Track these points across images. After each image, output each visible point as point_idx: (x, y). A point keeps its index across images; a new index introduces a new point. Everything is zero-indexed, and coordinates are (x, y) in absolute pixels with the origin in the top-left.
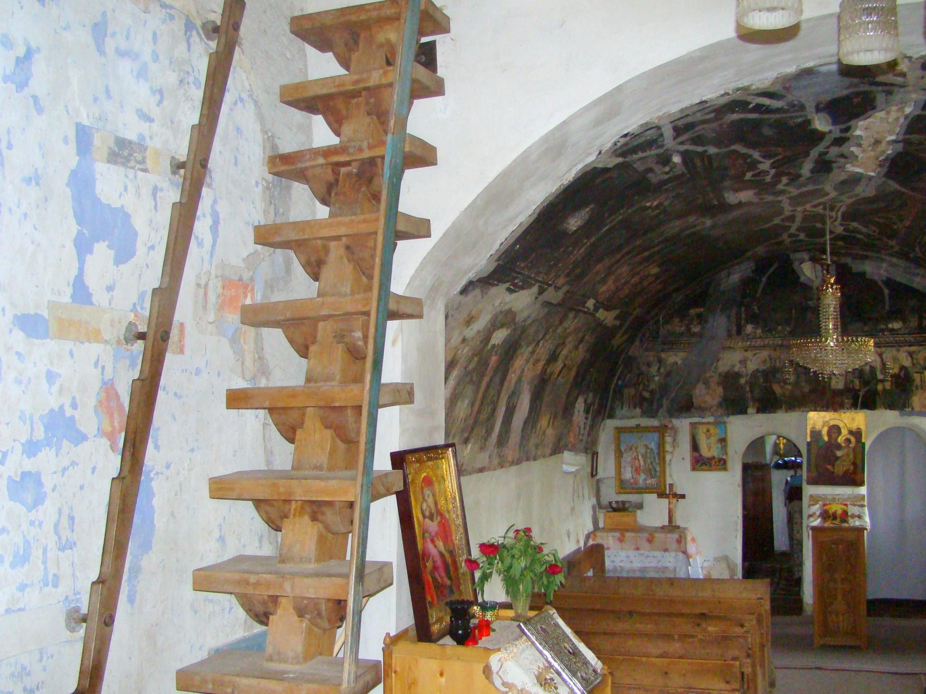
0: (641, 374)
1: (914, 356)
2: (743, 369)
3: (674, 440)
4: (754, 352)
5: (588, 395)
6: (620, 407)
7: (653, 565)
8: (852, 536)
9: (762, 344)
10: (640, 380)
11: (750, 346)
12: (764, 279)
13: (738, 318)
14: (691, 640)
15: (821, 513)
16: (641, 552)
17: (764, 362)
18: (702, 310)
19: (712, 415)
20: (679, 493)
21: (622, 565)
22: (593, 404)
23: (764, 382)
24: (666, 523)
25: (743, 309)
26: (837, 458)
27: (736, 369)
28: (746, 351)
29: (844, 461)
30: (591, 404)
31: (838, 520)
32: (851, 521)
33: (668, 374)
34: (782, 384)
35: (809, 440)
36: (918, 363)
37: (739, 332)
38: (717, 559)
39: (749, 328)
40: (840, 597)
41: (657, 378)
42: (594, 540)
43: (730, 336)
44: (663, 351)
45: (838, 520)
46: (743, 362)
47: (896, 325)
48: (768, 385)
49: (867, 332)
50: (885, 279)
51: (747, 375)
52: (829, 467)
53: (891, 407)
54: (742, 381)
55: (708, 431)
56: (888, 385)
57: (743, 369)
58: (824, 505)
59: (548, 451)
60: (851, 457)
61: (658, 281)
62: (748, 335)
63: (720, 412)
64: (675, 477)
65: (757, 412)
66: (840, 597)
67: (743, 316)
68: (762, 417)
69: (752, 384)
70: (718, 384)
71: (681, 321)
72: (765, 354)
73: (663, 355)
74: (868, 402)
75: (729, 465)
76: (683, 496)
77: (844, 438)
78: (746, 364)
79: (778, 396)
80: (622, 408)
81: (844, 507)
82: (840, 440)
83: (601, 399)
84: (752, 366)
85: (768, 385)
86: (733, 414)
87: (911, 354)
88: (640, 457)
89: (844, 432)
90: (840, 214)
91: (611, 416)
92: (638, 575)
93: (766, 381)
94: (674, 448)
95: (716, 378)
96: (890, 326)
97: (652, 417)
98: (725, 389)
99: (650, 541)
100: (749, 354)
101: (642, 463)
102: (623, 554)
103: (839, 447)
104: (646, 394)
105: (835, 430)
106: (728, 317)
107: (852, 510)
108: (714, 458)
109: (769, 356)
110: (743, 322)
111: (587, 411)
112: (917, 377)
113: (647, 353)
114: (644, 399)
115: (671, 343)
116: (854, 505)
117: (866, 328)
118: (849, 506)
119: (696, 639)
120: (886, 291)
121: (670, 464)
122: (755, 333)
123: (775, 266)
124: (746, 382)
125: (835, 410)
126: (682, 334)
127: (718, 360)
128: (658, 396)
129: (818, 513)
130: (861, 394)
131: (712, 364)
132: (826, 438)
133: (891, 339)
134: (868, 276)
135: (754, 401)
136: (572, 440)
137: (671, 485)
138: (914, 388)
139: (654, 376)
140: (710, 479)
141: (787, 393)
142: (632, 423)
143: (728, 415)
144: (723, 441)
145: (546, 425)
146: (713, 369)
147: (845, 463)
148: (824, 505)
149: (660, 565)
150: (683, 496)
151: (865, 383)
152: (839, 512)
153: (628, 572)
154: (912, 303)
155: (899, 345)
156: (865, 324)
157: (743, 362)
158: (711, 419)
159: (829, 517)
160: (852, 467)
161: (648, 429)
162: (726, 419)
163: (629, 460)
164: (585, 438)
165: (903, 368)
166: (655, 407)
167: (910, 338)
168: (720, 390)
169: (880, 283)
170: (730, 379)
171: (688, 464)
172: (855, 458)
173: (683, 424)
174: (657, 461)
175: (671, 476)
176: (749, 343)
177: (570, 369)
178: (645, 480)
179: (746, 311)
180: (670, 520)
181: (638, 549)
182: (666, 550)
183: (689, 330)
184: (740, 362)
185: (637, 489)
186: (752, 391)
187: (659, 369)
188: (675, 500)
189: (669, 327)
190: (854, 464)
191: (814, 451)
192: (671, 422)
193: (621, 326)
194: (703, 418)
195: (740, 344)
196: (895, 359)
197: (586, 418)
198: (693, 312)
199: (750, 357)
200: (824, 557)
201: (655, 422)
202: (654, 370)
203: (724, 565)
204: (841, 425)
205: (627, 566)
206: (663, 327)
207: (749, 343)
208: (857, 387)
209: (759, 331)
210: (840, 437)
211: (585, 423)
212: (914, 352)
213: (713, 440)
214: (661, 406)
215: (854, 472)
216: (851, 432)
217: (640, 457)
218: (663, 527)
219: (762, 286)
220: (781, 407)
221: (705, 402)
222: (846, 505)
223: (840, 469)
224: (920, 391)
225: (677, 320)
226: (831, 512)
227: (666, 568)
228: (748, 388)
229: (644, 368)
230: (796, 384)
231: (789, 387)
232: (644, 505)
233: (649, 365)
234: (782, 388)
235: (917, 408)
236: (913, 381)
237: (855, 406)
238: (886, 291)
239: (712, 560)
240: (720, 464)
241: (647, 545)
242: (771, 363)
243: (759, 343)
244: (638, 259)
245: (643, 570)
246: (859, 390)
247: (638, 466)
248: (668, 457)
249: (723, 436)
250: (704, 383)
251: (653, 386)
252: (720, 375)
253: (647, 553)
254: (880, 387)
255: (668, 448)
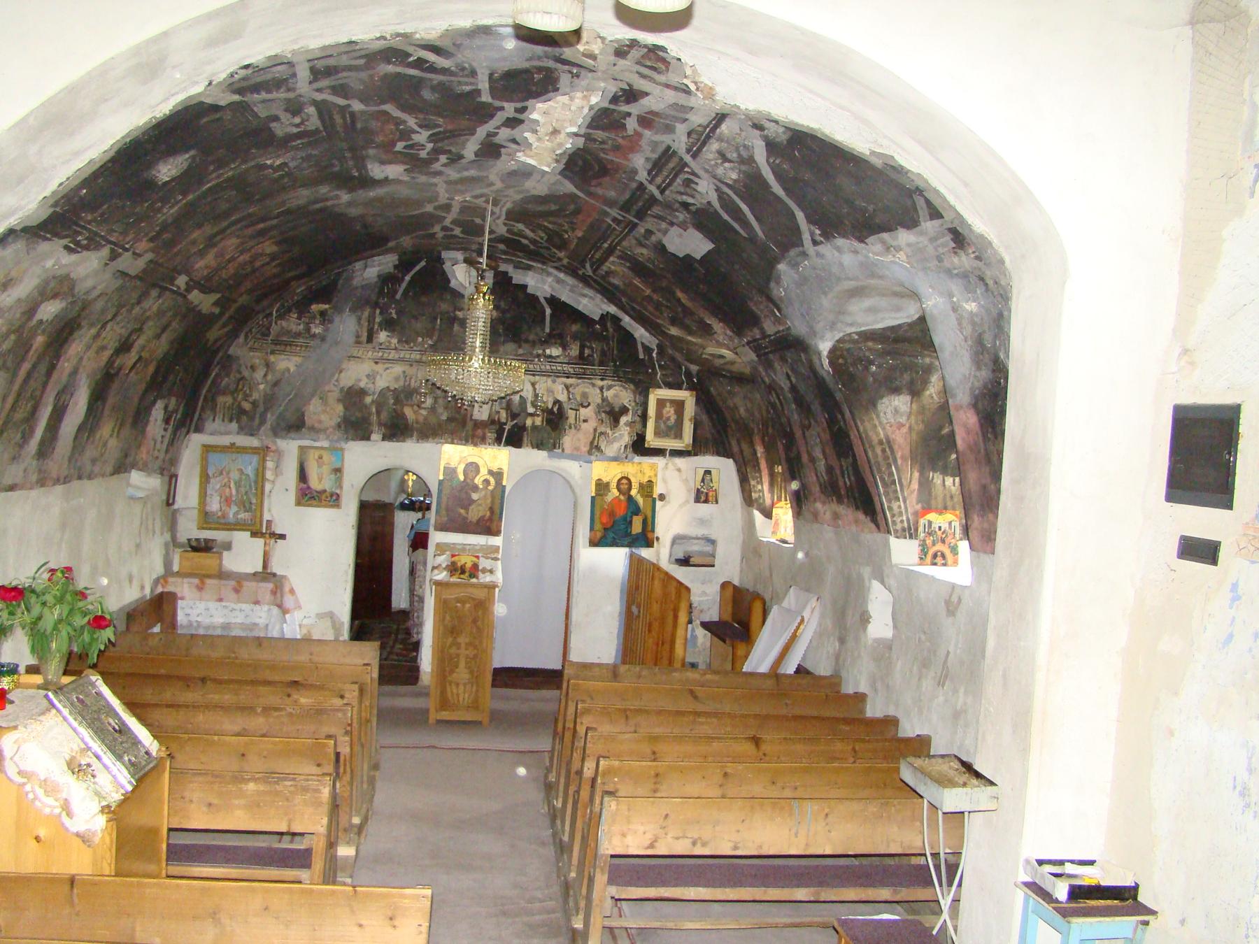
0: (243, 378)
1: (571, 389)
2: (371, 386)
3: (277, 467)
4: (386, 366)
5: (169, 400)
6: (212, 418)
7: (239, 620)
8: (480, 594)
9: (397, 356)
10: (240, 387)
11: (382, 358)
12: (408, 278)
13: (371, 320)
14: (276, 714)
15: (447, 566)
16: (224, 604)
17: (397, 379)
18: (327, 306)
19: (327, 438)
20: (278, 532)
21: (199, 619)
22: (176, 411)
23: (394, 404)
24: (260, 569)
25: (378, 311)
26: (474, 501)
27: (362, 385)
28: (376, 363)
29: (480, 505)
30: (173, 412)
31: (467, 574)
32: (481, 575)
33: (276, 384)
34: (415, 407)
35: (441, 477)
36: (575, 399)
37: (370, 339)
38: (320, 616)
39: (383, 336)
40: (462, 664)
41: (262, 387)
42: (163, 586)
43: (358, 342)
44: (273, 352)
45: (467, 574)
46: (371, 377)
47: (555, 351)
48: (398, 407)
49: (520, 355)
50: (548, 296)
51: (374, 393)
52: (462, 511)
53: (539, 446)
54: (368, 400)
55: (321, 457)
56: (538, 421)
57: (371, 386)
58: (453, 556)
59: (109, 469)
60: (489, 501)
61: (274, 264)
62: (381, 344)
63: (338, 434)
64: (274, 511)
65: (383, 439)
66: (462, 664)
67: (378, 320)
68: (387, 444)
69: (380, 405)
70: (339, 400)
71: (299, 318)
72: (398, 369)
73: (272, 358)
74: (514, 439)
75: (344, 500)
76: (282, 537)
77: (482, 479)
78: (374, 379)
79: (410, 421)
80: (214, 420)
81: (474, 559)
82: (478, 481)
83: (186, 405)
84: (381, 383)
85: (398, 407)
86: (353, 440)
87: (567, 387)
88: (232, 485)
89: (484, 471)
90: (504, 210)
91: (199, 429)
92: (219, 632)
93: (397, 401)
94: (277, 476)
95: (336, 394)
96: (548, 352)
97: (252, 435)
98: (346, 408)
99: (237, 591)
100: (380, 368)
101: (234, 492)
102: (201, 606)
103: (475, 488)
104: (247, 406)
105: (473, 468)
106: (359, 319)
107: (484, 563)
108: (325, 491)
109: (404, 372)
110: (376, 327)
111: (167, 421)
112: (571, 414)
113: (252, 354)
114: (242, 412)
115: (283, 343)
116: (487, 558)
117: (521, 351)
118: (482, 559)
119: (283, 713)
120: (548, 311)
121: (269, 496)
122: (390, 342)
123: (423, 263)
124: (373, 401)
125: (475, 445)
126: (298, 335)
127: (341, 372)
128: (261, 408)
129: (444, 566)
130: (507, 428)
131: (333, 375)
132: (462, 478)
133: (548, 367)
134: (529, 290)
135: (380, 424)
136: (144, 456)
137: (269, 522)
138: (567, 427)
139: (259, 384)
140: (319, 516)
141: (421, 419)
142: (225, 440)
143: (347, 439)
144: (338, 471)
145: (107, 436)
146: (333, 381)
147: (480, 508)
148: (453, 556)
149: (248, 621)
150: (282, 537)
151: (514, 416)
152: (469, 565)
153: (208, 628)
154: (575, 328)
155: (557, 374)
156: (520, 347)
157: (371, 377)
158: (326, 444)
159: (456, 570)
160: (488, 514)
161: (243, 450)
162: (343, 445)
163: (218, 486)
164: (162, 455)
165: (557, 402)
166: (257, 421)
167: (567, 368)
168: (340, 409)
169: (542, 301)
170: (353, 396)
171: (292, 496)
172: (493, 502)
173: (290, 447)
174: (254, 491)
175: (269, 510)
176: (380, 354)
177: (147, 362)
178: (236, 513)
179: (381, 313)
180: (265, 566)
181: (221, 600)
182: (257, 602)
183: (308, 330)
184: (368, 376)
185: (225, 524)
186: (378, 413)
187: (265, 375)
188: (273, 541)
189: (284, 323)
190: (491, 509)
191: (446, 491)
192: (275, 443)
193: (222, 314)
194: (315, 441)
195: (370, 353)
196: (550, 391)
197: (165, 430)
198: (315, 307)
199: (381, 371)
200: (448, 618)
201: (254, 442)
202: (259, 375)
203: (329, 623)
204: (480, 463)
205: (206, 621)
206: (276, 323)
207: (380, 354)
208: (503, 420)
209: (394, 341)
210: (478, 477)
211: (163, 437)
212: (571, 385)
213: (326, 469)
214: (263, 422)
215: (491, 519)
216: (491, 472)
217: (232, 485)
218: (255, 574)
219: (404, 285)
220: (412, 436)
221: (320, 422)
222: (478, 557)
223: (474, 514)
224: (573, 430)
225: (296, 315)
226: (459, 564)
227: (255, 624)
228: (374, 410)
229: (246, 373)
230: (433, 410)
231: (424, 412)
232: (233, 546)
233: (253, 368)
234: (415, 412)
235: (567, 451)
236: (567, 418)
237: (498, 441)
238: (548, 311)
239: (313, 615)
240: (333, 500)
241: (233, 595)
242: (405, 381)
243: (393, 355)
244: (249, 231)
245: (226, 626)
246: (505, 424)
247: (228, 494)
248: (268, 487)
249: (338, 465)
250: (321, 398)
251: (255, 396)
252: (342, 389)
253: (233, 605)
254: (529, 422)
255: (269, 475)
